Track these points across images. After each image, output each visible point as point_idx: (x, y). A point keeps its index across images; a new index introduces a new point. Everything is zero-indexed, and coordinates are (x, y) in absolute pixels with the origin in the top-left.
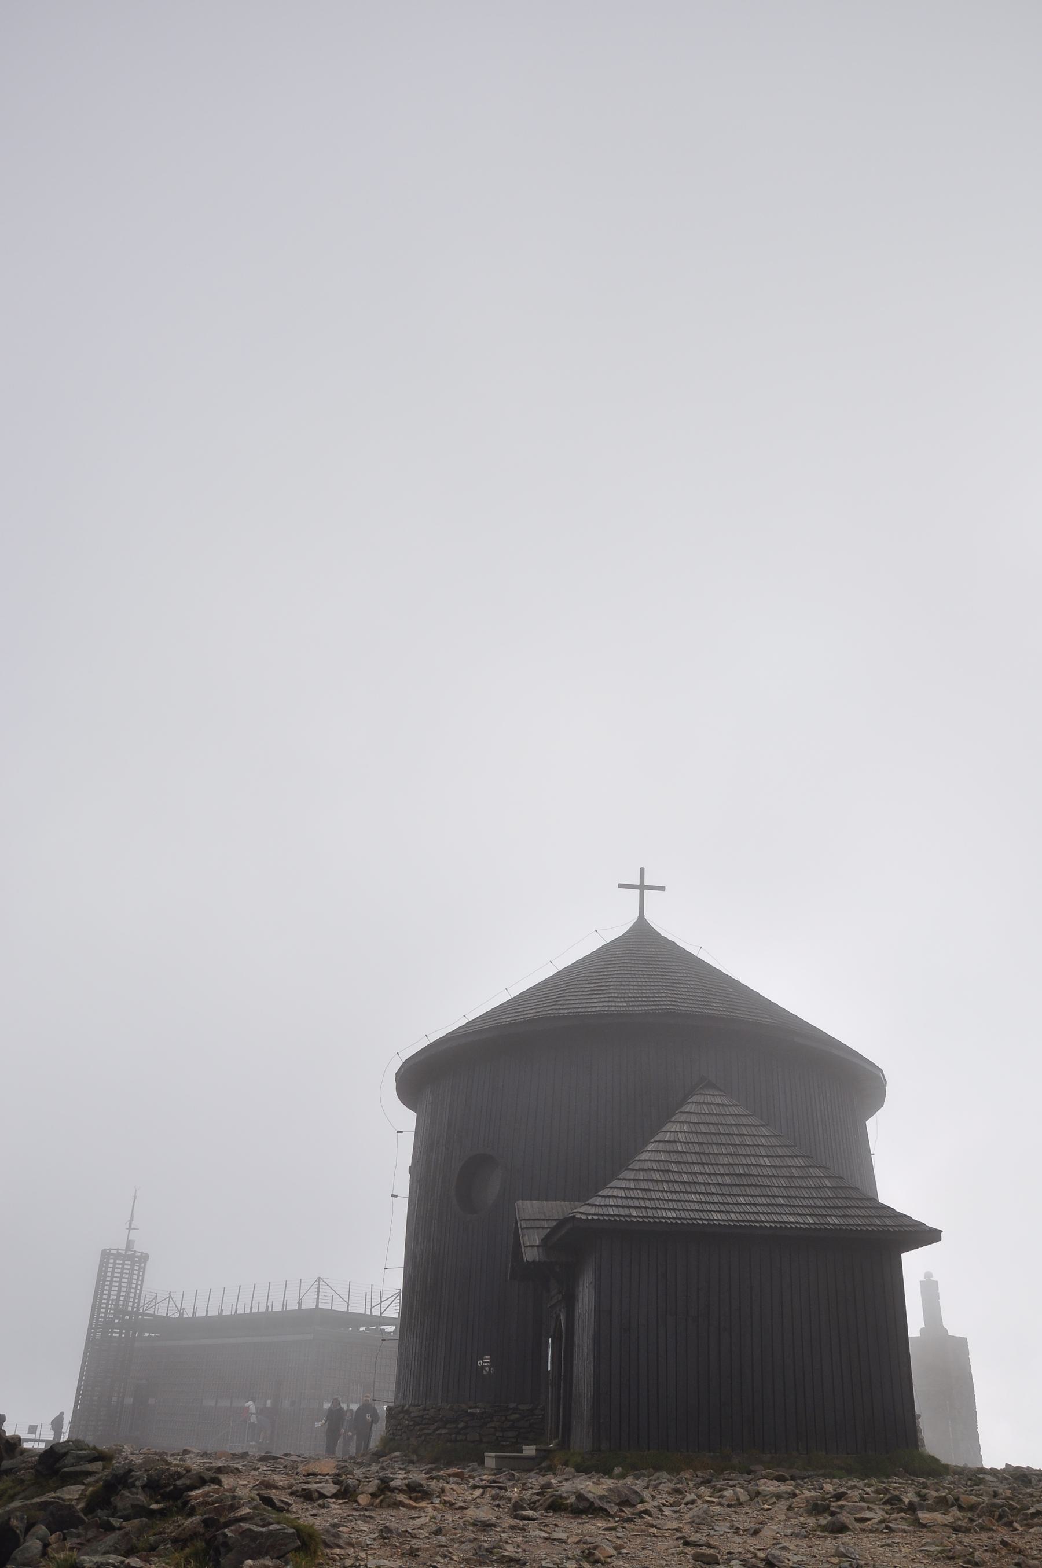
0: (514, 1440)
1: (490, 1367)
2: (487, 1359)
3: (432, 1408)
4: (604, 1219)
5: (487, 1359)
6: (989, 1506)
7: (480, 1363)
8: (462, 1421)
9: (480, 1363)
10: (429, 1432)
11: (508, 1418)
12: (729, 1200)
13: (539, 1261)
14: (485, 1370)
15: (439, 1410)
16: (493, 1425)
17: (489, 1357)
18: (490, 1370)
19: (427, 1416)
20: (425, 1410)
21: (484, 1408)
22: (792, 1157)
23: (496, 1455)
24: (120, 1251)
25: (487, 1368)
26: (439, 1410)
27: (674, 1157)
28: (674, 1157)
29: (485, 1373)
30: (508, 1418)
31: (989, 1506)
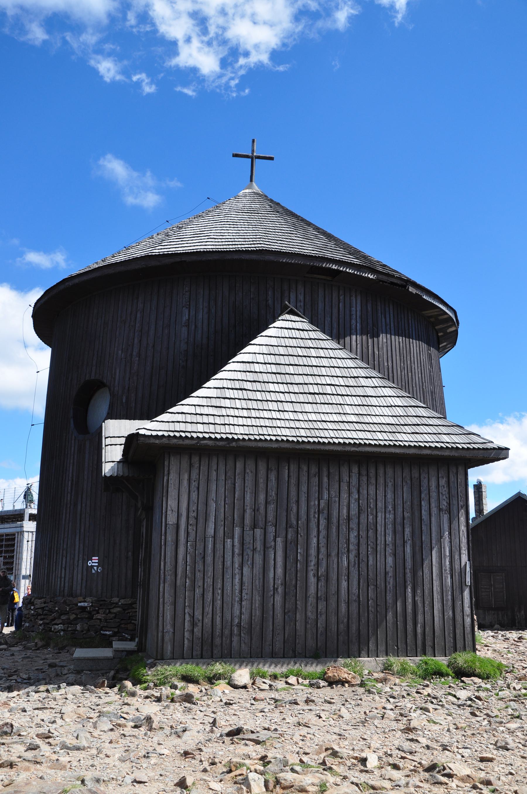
0: (116, 630)
1: (98, 567)
2: (95, 559)
3: (51, 602)
4: (181, 436)
5: (95, 559)
6: (206, 39)
7: (90, 563)
8: (73, 613)
9: (90, 563)
10: (48, 621)
11: (112, 611)
12: (300, 417)
13: (117, 476)
14: (94, 569)
15: (56, 603)
16: (99, 617)
17: (97, 558)
18: (97, 569)
19: (47, 609)
20: (45, 603)
21: (92, 603)
22: (367, 378)
23: (370, 338)
24: (424, 406)
25: (95, 568)
26: (56, 603)
27: (250, 377)
28: (250, 377)
29: (93, 572)
30: (112, 611)
31: (206, 39)
